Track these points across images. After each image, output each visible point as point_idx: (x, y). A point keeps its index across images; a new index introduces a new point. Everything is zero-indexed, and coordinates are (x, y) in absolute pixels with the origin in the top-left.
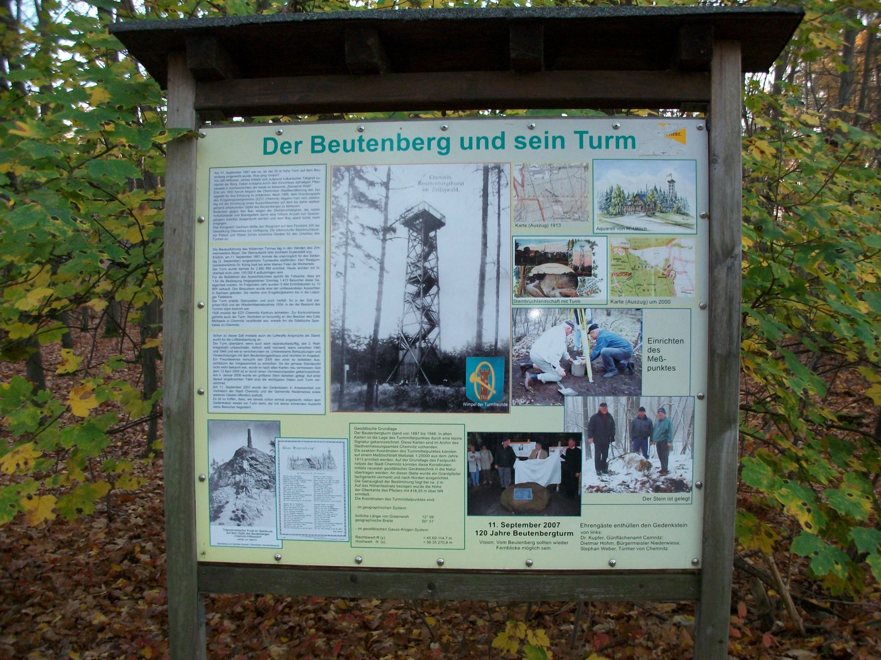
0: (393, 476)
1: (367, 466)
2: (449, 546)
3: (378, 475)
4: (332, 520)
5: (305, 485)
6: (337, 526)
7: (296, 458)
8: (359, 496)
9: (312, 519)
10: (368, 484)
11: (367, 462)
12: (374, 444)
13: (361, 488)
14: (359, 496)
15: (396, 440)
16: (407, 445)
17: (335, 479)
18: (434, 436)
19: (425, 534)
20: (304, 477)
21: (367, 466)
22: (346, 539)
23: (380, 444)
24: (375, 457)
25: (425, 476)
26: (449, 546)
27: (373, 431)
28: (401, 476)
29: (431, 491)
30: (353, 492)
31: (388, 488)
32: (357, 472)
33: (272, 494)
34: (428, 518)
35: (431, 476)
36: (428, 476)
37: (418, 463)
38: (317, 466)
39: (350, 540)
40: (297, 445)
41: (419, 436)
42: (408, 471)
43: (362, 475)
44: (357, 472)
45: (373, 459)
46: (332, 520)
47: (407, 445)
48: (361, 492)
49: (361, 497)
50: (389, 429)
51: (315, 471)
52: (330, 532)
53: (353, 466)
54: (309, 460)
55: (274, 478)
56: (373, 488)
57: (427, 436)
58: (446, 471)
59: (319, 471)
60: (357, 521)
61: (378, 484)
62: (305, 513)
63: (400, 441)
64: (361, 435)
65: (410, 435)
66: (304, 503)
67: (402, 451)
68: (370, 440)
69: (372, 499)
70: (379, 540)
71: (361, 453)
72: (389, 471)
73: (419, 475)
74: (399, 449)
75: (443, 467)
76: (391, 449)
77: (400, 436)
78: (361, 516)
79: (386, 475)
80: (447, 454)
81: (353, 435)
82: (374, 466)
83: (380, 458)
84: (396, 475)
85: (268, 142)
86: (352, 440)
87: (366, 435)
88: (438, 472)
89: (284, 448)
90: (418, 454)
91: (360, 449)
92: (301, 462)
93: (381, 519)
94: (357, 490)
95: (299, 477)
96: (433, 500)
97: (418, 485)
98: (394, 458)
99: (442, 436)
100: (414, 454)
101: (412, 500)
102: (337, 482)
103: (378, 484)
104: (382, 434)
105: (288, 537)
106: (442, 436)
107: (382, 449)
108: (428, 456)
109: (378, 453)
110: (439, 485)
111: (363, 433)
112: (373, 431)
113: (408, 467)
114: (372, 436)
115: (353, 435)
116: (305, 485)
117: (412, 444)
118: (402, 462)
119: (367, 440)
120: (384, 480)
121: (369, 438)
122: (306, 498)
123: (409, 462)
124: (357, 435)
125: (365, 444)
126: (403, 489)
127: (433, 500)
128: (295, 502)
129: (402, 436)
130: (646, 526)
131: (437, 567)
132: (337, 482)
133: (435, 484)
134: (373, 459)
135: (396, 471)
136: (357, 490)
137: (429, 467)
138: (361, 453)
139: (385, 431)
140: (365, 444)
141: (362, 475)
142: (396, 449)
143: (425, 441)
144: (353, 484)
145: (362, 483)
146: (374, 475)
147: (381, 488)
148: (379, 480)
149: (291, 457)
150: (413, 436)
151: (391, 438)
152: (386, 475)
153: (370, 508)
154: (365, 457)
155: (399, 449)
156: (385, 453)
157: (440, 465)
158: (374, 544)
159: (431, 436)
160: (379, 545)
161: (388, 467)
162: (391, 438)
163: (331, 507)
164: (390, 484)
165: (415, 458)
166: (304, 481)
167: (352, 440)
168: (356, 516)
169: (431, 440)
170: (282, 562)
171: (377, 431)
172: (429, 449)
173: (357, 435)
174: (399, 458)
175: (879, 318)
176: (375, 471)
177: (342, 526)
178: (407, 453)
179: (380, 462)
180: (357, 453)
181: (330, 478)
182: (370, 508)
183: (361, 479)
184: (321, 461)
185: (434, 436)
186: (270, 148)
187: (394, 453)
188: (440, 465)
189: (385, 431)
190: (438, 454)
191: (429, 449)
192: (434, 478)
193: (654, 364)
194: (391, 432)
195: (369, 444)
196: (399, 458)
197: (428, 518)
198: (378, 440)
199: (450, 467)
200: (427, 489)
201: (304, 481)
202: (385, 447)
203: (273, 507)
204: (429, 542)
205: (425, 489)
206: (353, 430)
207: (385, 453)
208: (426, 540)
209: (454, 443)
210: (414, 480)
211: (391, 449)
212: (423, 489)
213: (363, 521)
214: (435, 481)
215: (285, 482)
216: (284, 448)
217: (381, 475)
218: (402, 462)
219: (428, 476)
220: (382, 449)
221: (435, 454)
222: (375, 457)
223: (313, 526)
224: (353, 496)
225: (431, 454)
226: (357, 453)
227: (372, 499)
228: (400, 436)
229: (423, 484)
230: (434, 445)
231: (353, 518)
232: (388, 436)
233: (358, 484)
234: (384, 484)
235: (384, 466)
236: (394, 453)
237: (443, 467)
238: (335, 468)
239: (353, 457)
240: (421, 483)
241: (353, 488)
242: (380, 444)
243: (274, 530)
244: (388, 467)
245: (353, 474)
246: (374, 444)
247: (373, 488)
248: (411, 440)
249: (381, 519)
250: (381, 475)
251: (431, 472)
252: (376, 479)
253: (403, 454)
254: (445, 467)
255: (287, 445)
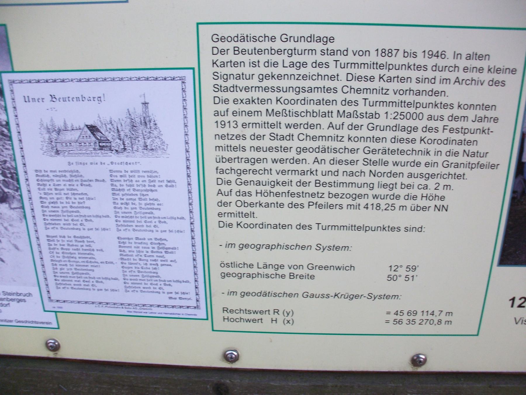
0: (321, 168)
1: (248, 143)
2: (443, 329)
3: (279, 167)
4: (164, 273)
5: (91, 192)
6: (176, 287)
7: (59, 124)
8: (227, 220)
9: (115, 271)
10: (252, 188)
11: (248, 132)
12: (266, 83)
13: (233, 198)
14: (227, 220)
15: (332, 71)
16: (363, 85)
17: (164, 177)
18: (441, 63)
19: (393, 305)
20: (88, 172)
21: (248, 143)
22: (201, 313)
23: (284, 83)
24: (273, 119)
25: (406, 170)
26: (443, 329)
27: (267, 45)
28: (343, 168)
29: (417, 208)
30: (213, 210)
31: (305, 201)
32: (222, 160)
33: (15, 214)
34: (402, 272)
35: (422, 169)
36: (416, 170)
37: (389, 134)
38: (116, 144)
39: (209, 316)
40: (58, 90)
41: (399, 60)
42: (360, 156)
43: (236, 165)
44: (222, 160)
45: (266, 125)
46: (164, 273)
47: (363, 85)
48: (233, 209)
49: (234, 220)
50: (311, 38)
51: (114, 157)
52: (163, 299)
53: (210, 142)
54: (93, 129)
55: (15, 176)
56: (264, 200)
57: (420, 61)
58: (461, 159)
59: (122, 158)
60: (224, 276)
61: (278, 189)
62: (99, 257)
63: (343, 73)
64: (230, 57)
65: (373, 58)
66: (93, 235)
67: (347, 102)
68: (256, 71)
69: (262, 226)
70: (280, 318)
71: (232, 107)
72: (310, 157)
73: (390, 168)
74: (339, 97)
75: (455, 148)
76: (316, 96)
77: (343, 59)
78: (233, 265)
79: (300, 167)
80: (471, 114)
81: (207, 58)
82: (266, 143)
83: (284, 120)
84: (327, 167)
85: (215, 98)
86: (207, 70)
87: (246, 58)
88: (440, 159)
89: (27, 100)
90: (391, 110)
91: (230, 96)
92: (76, 135)
93: (286, 271)
94: (222, 204)
95: (75, 174)
96: (420, 229)
97: (386, 191)
98: (325, 122)
99: (462, 63)
100: (381, 110)
101: (366, 229)
102: (171, 183)
103: (278, 189)
104: (292, 52)
105: (66, 307)
106: (462, 63)
107: (291, 95)
108: (419, 117)
109: (279, 107)
110: (440, 193)
111: (236, 51)
112: (267, 45)
113: (361, 145)
114: (263, 58)
115: (207, 58)
116: (91, 192)
117: (377, 84)
118: (345, 132)
119: (248, 70)
120: (296, 178)
121: (254, 64)
122: (97, 223)
123: (364, 132)
124: (221, 58)
125: (241, 83)
126: (345, 202)
127: (420, 229)
128: (72, 233)
129: (351, 58)
130: (304, 227)
131: (409, 368)
132: (171, 183)
133: (431, 191)
134: (266, 125)
135: (328, 156)
136: (222, 204)
137: (418, 146)
138: (232, 107)
139: (302, 46)
140: (241, 83)
141: (236, 165)
142: (330, 96)
143: (414, 74)
144: (212, 188)
145: (235, 188)
146: (269, 165)
147: (286, 200)
148: (281, 178)
149: (47, 122)
150: (381, 60)
151: (317, 64)
152: (300, 167)
153: (258, 247)
154: (241, 120)
155: (339, 97)
156: (299, 108)
157: (447, 141)
158: (266, 325)
159: (431, 62)
160: (280, 327)
161: (308, 144)
162: (317, 64)
163: (160, 242)
164: (312, 189)
165: (382, 121)
166: (87, 183)
167: (207, 70)
168: (223, 265)
169: (430, 74)
170: (63, 354)
171: (278, 45)
172: (424, 99)
173: (221, 58)
174: (337, 121)
175: (1, 305)
176: (270, 155)
177: (190, 288)
178: (361, 109)
179: (285, 132)
180: (222, 107)
181: (152, 174)
182: (258, 247)
183: (233, 177)
184: (126, 130)
185: (441, 63)
186: (217, 101)
187: (324, 108)
188: (447, 141)
189: (302, 46)
190: (447, 113)
191: (424, 99)
192: (433, 176)
193: (163, 263)
194: (319, 46)
195: (255, 82)
196: (337, 121)
197: (402, 272)
198: (279, 70)
199: (473, 148)
200: (409, 203)
201: (87, 183)
202: (299, 90)
203: (23, 244)
204: (400, 322)
205: (402, 202)
206: (207, 45)
207: (299, 108)
208: (392, 317)
209: (495, 83)
210: (375, 180)
211: (316, 96)
212: (398, 203)
213: (240, 276)
214: (431, 183)
215: (41, 184)
216: (27, 100)
217: (287, 166)
218: (345, 132)
219: (416, 170)
220: (291, 95)
221: (436, 112)
222: (273, 119)
223: (119, 285)
224: (213, 220)
225: (427, 112)
226: (222, 107)
227: (262, 226)
228: (343, 59)
229: (397, 191)
230: (438, 87)
231: (216, 271)
232: (309, 59)
233: (225, 188)
234: (294, 189)
235: (295, 144)
236: (324, 108)
237: (455, 148)
238: (163, 147)
239: (209, 119)
240: (392, 187)
241: (212, 199)
242: (284, 83)
243: (35, 291)
244: (308, 144)
245: (210, 165)
246: (266, 83)
247: (264, 200)
248: (376, 73)
249: (286, 271)
250: (287, 166)
251: (423, 159)
252: (274, 177)
253: (349, 109)
254: (460, 149)
255: (34, 90)
